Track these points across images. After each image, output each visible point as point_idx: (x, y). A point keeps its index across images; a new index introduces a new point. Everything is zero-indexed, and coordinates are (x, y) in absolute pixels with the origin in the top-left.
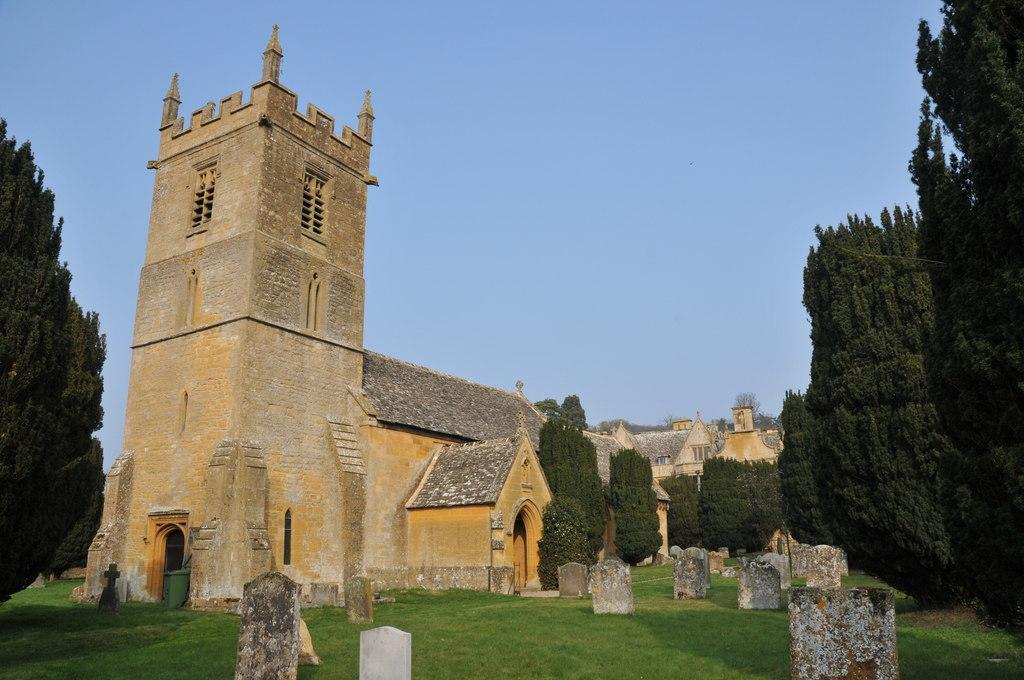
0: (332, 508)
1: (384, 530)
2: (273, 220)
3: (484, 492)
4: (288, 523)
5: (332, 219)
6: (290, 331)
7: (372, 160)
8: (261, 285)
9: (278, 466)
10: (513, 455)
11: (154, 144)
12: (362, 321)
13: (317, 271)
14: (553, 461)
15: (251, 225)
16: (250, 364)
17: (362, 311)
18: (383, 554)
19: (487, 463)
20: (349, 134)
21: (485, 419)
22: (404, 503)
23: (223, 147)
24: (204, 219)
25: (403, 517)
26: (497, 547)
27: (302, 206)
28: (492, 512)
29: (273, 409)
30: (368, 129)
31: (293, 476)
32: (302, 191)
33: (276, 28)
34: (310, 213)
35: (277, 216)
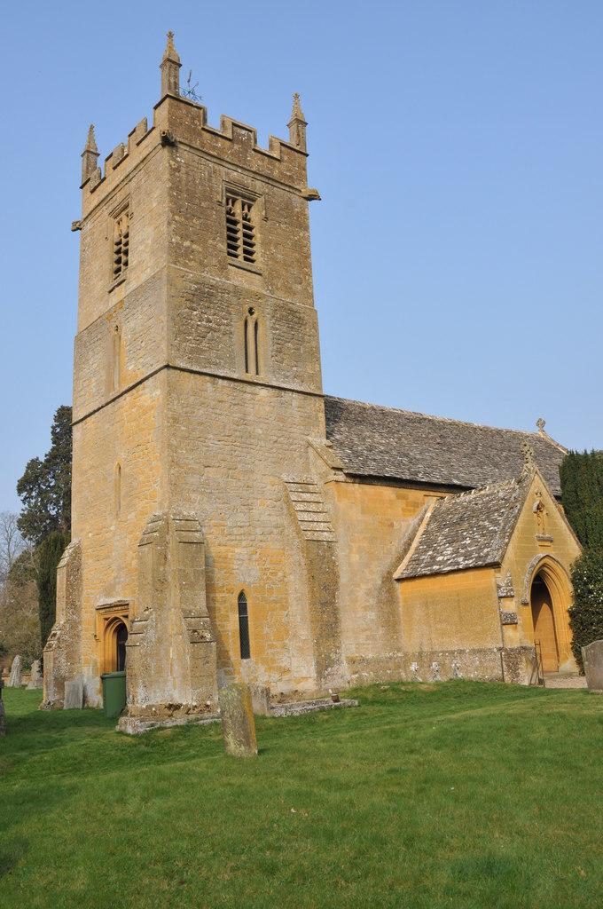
0: (297, 586)
1: (366, 608)
2: (189, 251)
3: (486, 550)
4: (242, 608)
5: (265, 244)
6: (223, 378)
7: (309, 172)
8: (180, 327)
9: (222, 540)
10: (522, 500)
11: (77, 203)
12: (318, 360)
13: (253, 305)
14: (580, 503)
15: (163, 260)
16: (176, 420)
17: (318, 348)
18: (368, 638)
19: (489, 512)
20: (277, 145)
21: (496, 465)
22: (390, 573)
23: (133, 184)
24: (123, 268)
25: (391, 591)
26: (509, 621)
27: (225, 233)
28: (497, 575)
29: (211, 472)
30: (300, 137)
31: (244, 551)
32: (224, 216)
33: (171, 35)
34: (238, 240)
35: (194, 246)
